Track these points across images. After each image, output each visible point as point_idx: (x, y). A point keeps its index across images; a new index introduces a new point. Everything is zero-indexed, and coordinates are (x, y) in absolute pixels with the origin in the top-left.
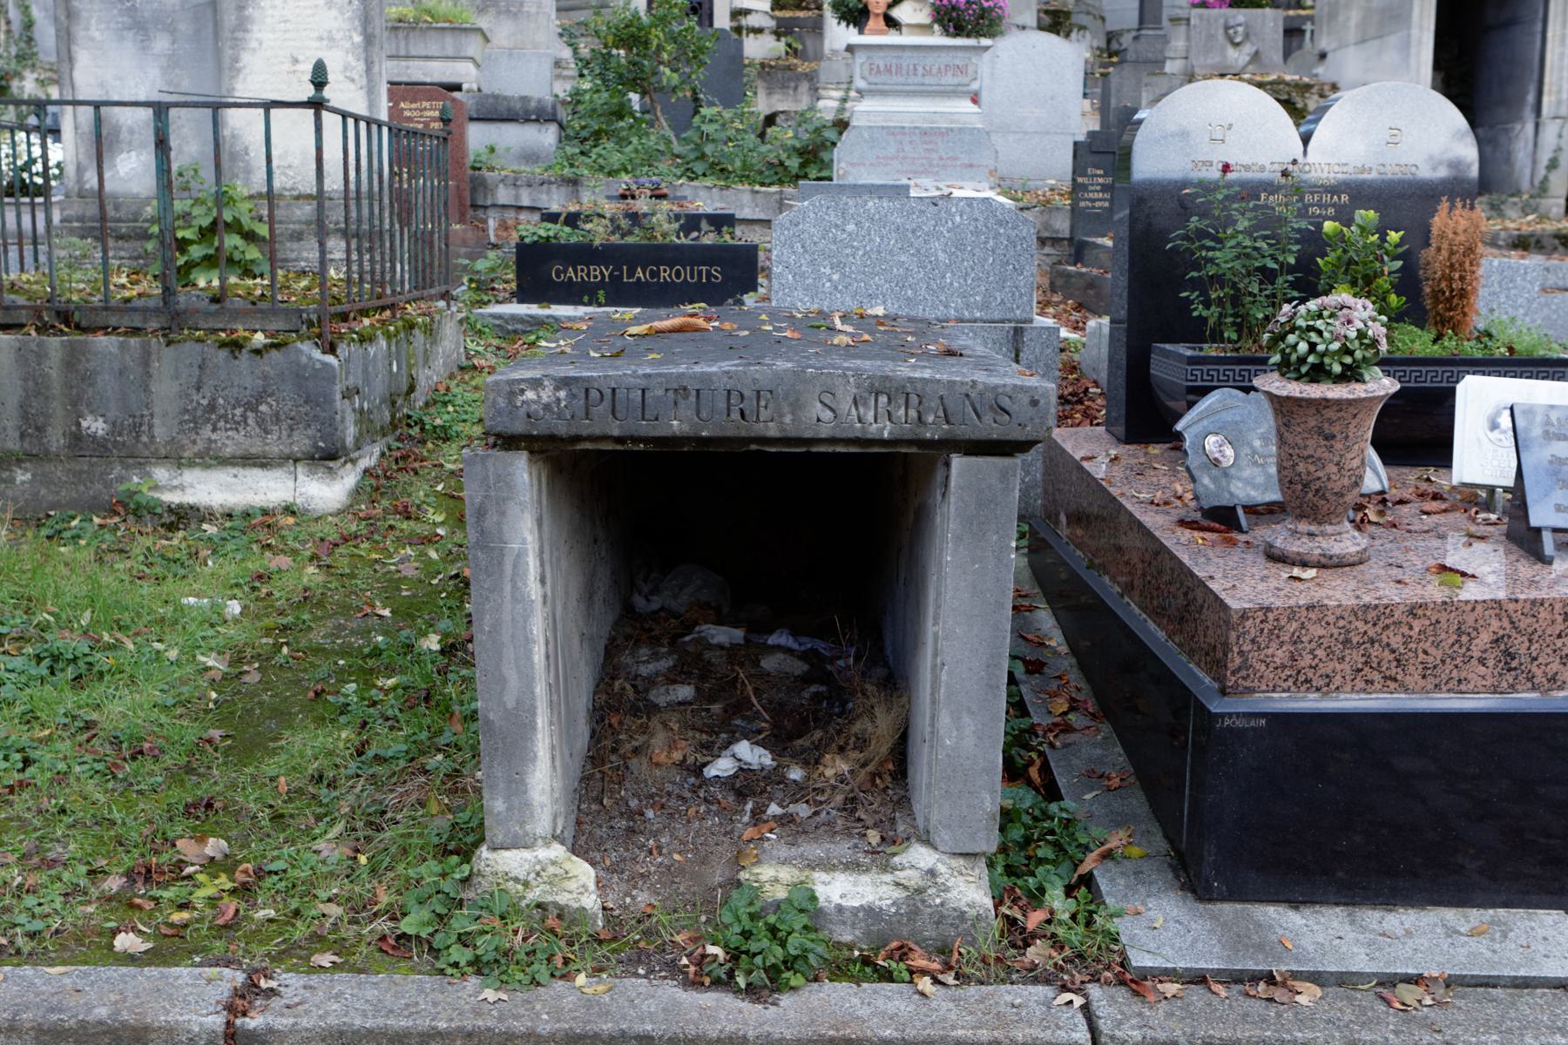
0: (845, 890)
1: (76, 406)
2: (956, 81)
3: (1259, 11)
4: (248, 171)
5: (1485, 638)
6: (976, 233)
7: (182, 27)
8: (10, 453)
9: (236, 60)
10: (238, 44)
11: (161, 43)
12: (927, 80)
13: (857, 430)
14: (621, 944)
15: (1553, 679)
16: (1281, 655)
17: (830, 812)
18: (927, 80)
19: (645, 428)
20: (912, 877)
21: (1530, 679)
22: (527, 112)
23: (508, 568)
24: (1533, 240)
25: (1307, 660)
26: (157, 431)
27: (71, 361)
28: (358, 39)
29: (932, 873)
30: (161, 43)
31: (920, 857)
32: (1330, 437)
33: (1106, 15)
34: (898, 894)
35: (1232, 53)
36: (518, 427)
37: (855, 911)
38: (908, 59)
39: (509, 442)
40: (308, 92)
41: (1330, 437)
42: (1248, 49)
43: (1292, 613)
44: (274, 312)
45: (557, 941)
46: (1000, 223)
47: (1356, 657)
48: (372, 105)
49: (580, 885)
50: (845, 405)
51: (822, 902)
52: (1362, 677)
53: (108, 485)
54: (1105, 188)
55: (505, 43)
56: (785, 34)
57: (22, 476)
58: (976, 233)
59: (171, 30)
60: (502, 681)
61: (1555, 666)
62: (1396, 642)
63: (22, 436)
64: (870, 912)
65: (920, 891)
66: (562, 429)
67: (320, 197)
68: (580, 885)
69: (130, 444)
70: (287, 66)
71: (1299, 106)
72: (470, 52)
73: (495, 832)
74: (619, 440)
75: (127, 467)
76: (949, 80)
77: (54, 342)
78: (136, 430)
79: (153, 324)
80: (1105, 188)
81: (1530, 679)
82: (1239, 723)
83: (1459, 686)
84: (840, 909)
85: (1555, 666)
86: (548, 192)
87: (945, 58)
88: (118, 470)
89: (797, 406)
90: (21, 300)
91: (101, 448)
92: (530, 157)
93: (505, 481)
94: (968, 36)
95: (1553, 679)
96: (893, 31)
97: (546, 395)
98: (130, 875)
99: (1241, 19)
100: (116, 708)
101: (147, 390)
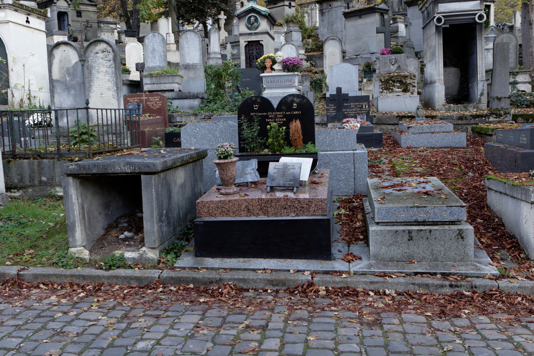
0: (129, 255)
1: (40, 175)
2: (289, 84)
3: (400, 55)
4: (92, 120)
5: (244, 206)
6: (225, 129)
7: (77, 88)
8: (27, 185)
9: (89, 95)
10: (89, 91)
11: (73, 92)
12: (282, 84)
13: (124, 171)
14: (91, 264)
15: (258, 214)
16: (206, 210)
17: (137, 243)
18: (282, 84)
19: (89, 172)
20: (141, 252)
21: (253, 214)
22: (190, 96)
23: (70, 197)
24: (464, 117)
25: (211, 211)
26: (57, 180)
27: (39, 165)
28: (115, 88)
29: (144, 251)
30: (73, 92)
31: (144, 249)
32: (223, 170)
33: (415, 47)
34: (138, 255)
35: (392, 67)
36: (69, 173)
37: (131, 258)
38: (276, 79)
39: (69, 175)
40: (85, 106)
41: (223, 170)
42: (396, 65)
43: (207, 202)
44: (80, 153)
45: (79, 262)
46: (230, 127)
47: (220, 210)
48: (119, 104)
49: (86, 254)
50: (122, 167)
51: (125, 257)
52: (222, 213)
53: (47, 192)
54: (334, 109)
55: (192, 77)
56: (310, 60)
57: (30, 190)
58: (225, 129)
59: (75, 89)
60: (70, 217)
61: (258, 211)
62: (227, 207)
63: (30, 181)
64: (133, 258)
65: (142, 254)
66: (76, 173)
67: (98, 125)
68: (86, 254)
69: (51, 183)
70: (100, 96)
71: (404, 82)
72: (176, 81)
73: (71, 245)
74: (86, 174)
75: (51, 188)
76: (287, 83)
77: (36, 161)
78: (52, 179)
79: (57, 157)
80: (334, 109)
81: (253, 214)
82: (198, 223)
83: (240, 215)
84: (128, 258)
85: (258, 211)
86: (190, 118)
87: (286, 78)
88: (49, 188)
89: (114, 167)
90: (30, 152)
91: (46, 184)
92: (191, 108)
93: (68, 182)
94: (291, 72)
95: (258, 214)
96: (273, 72)
97: (73, 167)
98: (14, 255)
99: (394, 57)
100: (27, 232)
101: (54, 171)
